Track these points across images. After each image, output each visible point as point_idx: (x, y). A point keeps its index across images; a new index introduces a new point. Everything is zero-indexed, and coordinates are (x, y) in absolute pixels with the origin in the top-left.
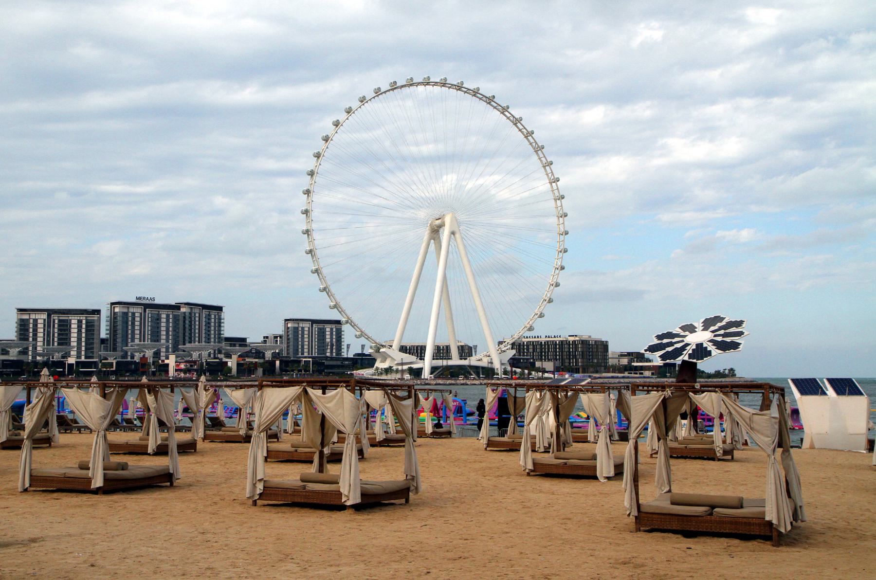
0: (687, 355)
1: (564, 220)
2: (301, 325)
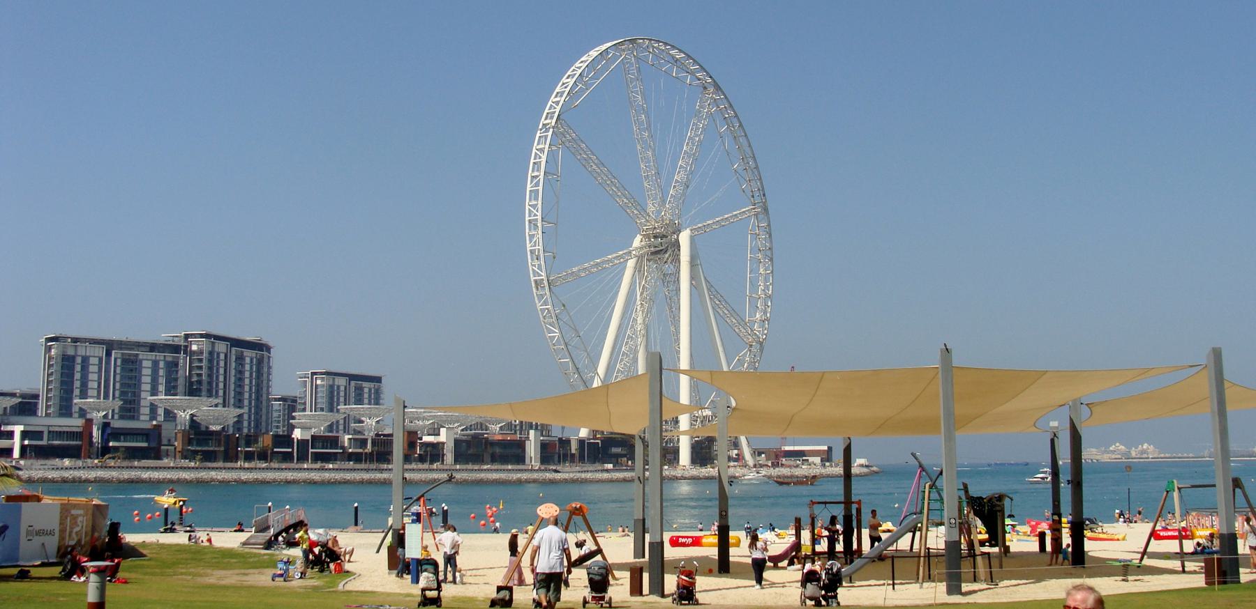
1: (1195, 572)
2: (81, 352)
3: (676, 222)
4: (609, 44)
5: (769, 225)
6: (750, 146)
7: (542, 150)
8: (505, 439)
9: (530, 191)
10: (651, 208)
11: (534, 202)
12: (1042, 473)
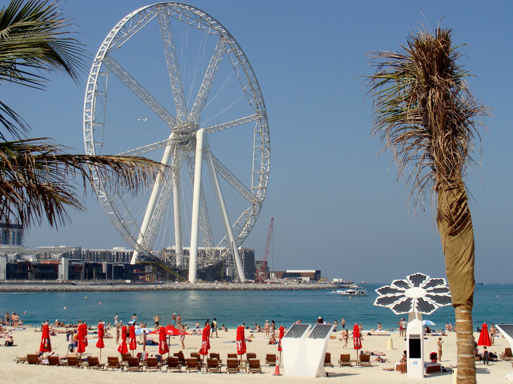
0: (426, 280)
3: (196, 124)
4: (147, 7)
5: (268, 127)
6: (254, 74)
7: (94, 76)
8: (46, 263)
9: (87, 103)
10: (179, 115)
11: (88, 110)
12: (352, 289)
